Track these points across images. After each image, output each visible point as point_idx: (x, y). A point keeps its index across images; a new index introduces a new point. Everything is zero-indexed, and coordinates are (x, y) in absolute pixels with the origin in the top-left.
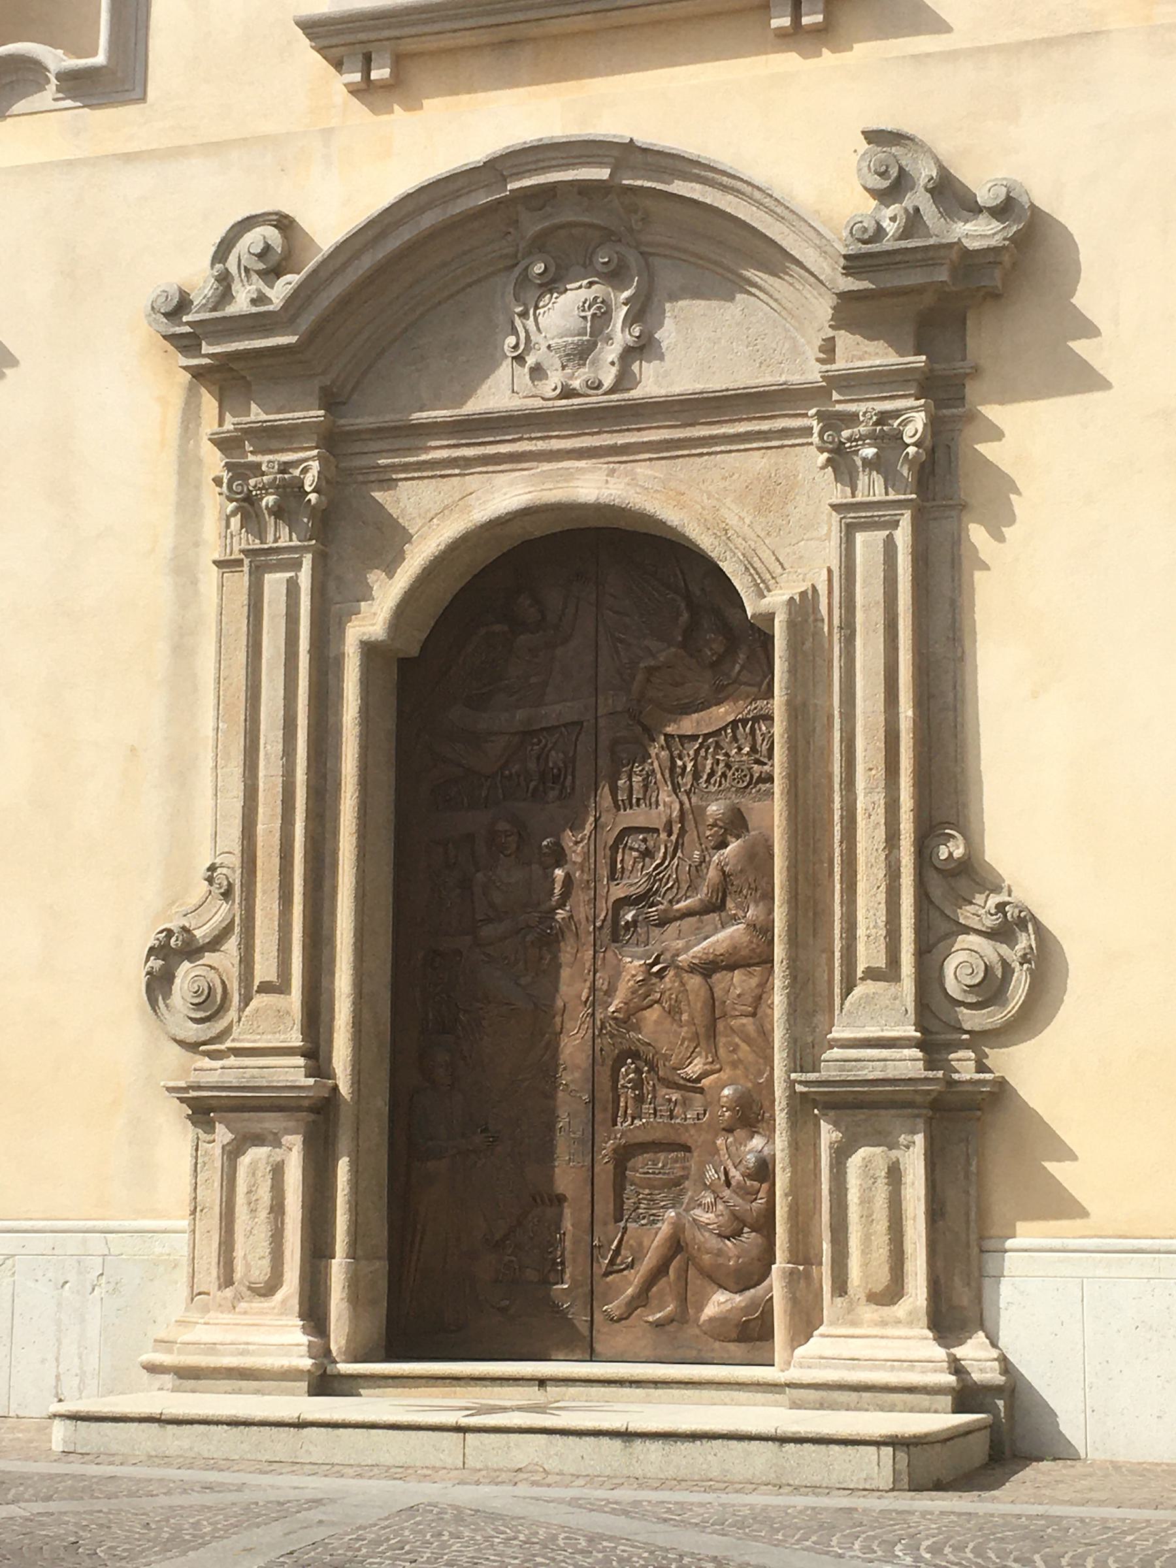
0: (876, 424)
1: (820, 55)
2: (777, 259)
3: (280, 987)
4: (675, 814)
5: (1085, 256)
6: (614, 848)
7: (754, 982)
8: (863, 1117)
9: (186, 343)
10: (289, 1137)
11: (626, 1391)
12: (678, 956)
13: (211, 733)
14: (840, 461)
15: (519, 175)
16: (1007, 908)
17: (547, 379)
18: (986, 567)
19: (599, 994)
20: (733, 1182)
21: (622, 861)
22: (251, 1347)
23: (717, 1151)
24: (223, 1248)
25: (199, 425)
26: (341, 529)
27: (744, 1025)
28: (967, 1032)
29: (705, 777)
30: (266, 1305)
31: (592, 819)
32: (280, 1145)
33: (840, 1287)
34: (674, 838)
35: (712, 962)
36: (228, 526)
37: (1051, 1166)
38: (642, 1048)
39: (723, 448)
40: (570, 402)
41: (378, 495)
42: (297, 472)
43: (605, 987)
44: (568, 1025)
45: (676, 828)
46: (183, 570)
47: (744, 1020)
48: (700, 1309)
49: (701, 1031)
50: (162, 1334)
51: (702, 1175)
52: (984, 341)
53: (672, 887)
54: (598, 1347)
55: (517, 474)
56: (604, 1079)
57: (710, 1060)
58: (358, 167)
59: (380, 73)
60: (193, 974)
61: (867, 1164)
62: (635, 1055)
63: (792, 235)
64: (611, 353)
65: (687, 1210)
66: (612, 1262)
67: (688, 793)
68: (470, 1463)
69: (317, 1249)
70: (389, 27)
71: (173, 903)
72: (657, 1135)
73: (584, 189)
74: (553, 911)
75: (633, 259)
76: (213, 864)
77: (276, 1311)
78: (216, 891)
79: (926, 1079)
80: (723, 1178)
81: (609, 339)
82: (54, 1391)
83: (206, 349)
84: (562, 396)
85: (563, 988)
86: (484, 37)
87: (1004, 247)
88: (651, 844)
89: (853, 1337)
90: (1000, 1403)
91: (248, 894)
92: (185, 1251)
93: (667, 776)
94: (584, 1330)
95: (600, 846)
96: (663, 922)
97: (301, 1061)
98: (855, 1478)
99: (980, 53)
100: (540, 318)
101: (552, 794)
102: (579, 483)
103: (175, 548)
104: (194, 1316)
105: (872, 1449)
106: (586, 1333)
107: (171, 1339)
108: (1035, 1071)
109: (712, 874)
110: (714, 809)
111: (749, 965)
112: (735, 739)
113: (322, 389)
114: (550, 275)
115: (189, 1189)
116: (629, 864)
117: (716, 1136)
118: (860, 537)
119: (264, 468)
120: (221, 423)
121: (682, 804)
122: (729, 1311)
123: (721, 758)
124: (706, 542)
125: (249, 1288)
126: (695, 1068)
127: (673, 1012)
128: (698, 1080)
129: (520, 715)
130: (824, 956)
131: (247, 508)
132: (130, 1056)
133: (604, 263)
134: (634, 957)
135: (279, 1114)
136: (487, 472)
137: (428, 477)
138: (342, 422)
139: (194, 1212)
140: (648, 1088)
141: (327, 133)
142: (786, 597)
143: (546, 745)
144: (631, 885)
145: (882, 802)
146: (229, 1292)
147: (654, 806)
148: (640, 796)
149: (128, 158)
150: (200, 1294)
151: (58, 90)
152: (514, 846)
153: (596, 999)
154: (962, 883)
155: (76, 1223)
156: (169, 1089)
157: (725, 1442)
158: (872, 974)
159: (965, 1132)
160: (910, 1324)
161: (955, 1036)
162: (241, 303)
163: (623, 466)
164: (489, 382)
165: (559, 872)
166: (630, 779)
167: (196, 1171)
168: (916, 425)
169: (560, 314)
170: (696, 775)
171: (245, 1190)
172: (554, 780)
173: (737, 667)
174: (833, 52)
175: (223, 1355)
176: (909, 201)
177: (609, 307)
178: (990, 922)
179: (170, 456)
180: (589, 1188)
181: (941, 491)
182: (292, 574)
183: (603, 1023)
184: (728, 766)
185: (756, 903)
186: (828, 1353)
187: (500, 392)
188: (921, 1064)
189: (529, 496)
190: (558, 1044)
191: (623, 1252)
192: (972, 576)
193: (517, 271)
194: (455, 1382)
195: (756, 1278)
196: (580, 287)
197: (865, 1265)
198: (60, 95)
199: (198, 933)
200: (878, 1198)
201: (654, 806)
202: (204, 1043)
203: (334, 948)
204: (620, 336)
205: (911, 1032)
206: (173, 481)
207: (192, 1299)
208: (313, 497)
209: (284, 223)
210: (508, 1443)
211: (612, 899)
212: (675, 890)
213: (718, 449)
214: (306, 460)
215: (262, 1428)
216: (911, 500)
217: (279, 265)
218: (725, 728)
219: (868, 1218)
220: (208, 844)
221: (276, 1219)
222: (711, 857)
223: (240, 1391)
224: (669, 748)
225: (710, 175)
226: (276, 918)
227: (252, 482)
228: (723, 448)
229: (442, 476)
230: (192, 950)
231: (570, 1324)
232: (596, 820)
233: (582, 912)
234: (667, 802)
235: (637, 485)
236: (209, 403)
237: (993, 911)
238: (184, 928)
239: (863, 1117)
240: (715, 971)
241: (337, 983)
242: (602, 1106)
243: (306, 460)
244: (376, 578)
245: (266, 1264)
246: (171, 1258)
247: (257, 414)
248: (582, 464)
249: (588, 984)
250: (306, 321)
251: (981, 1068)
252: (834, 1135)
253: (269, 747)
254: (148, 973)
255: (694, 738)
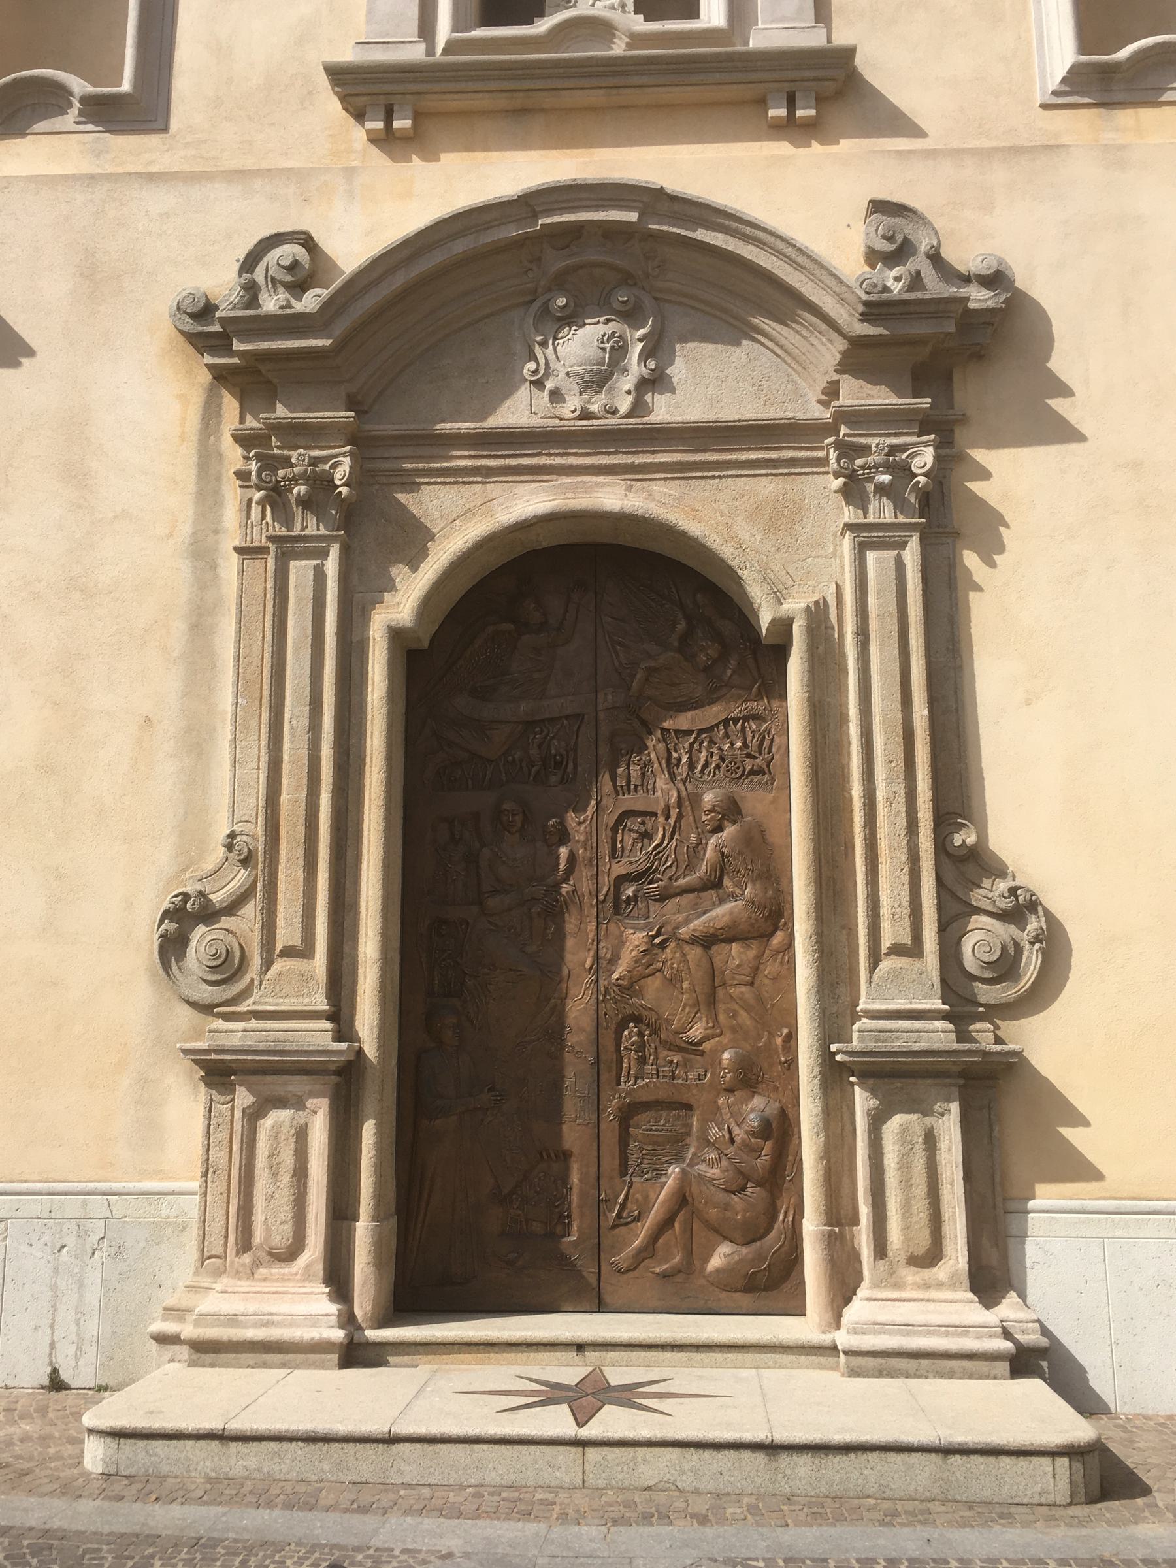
0: (888, 454)
1: (809, 146)
2: (786, 303)
3: (304, 951)
4: (673, 800)
5: (1059, 328)
6: (615, 830)
7: (752, 953)
8: (899, 1085)
9: (201, 342)
10: (315, 1101)
11: (668, 1355)
12: (678, 928)
13: (229, 708)
14: (853, 491)
15: (549, 212)
16: (1019, 892)
17: (564, 401)
18: (979, 589)
19: (604, 963)
20: (738, 1139)
21: (622, 841)
22: (275, 1318)
23: (719, 1109)
24: (241, 1213)
25: (219, 423)
26: (372, 531)
27: (742, 993)
28: (982, 1005)
29: (699, 768)
30: (286, 1271)
31: (593, 802)
32: (304, 1108)
33: (881, 1250)
34: (672, 821)
35: (712, 935)
36: (248, 516)
37: (1066, 1132)
38: (645, 1013)
39: (734, 472)
40: (591, 422)
41: (401, 497)
42: (327, 467)
43: (608, 956)
44: (571, 992)
45: (674, 813)
46: (202, 555)
47: (743, 989)
48: (706, 1259)
49: (702, 998)
50: (171, 1302)
51: (704, 1131)
52: (969, 392)
53: (671, 866)
54: (608, 1298)
55: (538, 484)
56: (608, 1041)
57: (710, 1025)
58: (377, 207)
59: (401, 124)
60: (210, 938)
61: (904, 1129)
62: (638, 1020)
63: (810, 283)
64: (627, 382)
65: (691, 1165)
66: (619, 1216)
67: (684, 781)
68: (591, 1480)
69: (341, 1212)
70: (415, 81)
71: (188, 868)
72: (661, 1095)
73: (611, 231)
74: (557, 886)
75: (647, 301)
76: (233, 831)
77: (298, 1277)
78: (234, 856)
79: (955, 1051)
80: (727, 1136)
81: (625, 370)
82: (47, 1360)
83: (237, 345)
84: (580, 418)
85: (569, 957)
86: (502, 102)
87: (1000, 309)
88: (649, 827)
89: (899, 1300)
90: (1044, 1364)
91: (271, 862)
92: (195, 1213)
93: (664, 765)
94: (593, 1280)
95: (602, 828)
96: (663, 898)
97: (328, 1025)
98: (1029, 1492)
99: (957, 154)
100: (559, 348)
101: (554, 779)
102: (596, 494)
103: (194, 534)
104: (205, 1281)
105: (1046, 1461)
106: (595, 1284)
107: (183, 1307)
108: (1049, 1043)
109: (710, 853)
110: (709, 798)
111: (747, 939)
112: (727, 735)
113: (348, 396)
114: (567, 312)
115: (200, 1150)
116: (629, 843)
117: (718, 1096)
118: (871, 556)
119: (293, 461)
120: (242, 420)
121: (679, 792)
122: (737, 1263)
123: (715, 751)
124: (726, 552)
125: (270, 1254)
126: (697, 1031)
127: (673, 981)
128: (700, 1043)
129: (523, 707)
130: (844, 932)
131: (276, 497)
132: (126, 1005)
133: (623, 302)
134: (636, 929)
135: (305, 1077)
136: (507, 482)
137: (450, 483)
138: (367, 427)
139: (205, 1174)
140: (650, 1049)
141: (350, 172)
142: (803, 605)
143: (548, 735)
144: (631, 863)
145: (903, 791)
146: (247, 1258)
147: (651, 792)
148: (638, 783)
149: (152, 178)
150: (210, 1258)
151: (81, 114)
152: (519, 825)
153: (601, 965)
154: (970, 869)
155: (76, 1184)
156: (186, 1052)
157: (883, 1455)
158: (897, 950)
159: (999, 1114)
160: (953, 1285)
161: (973, 1009)
162: (271, 304)
163: (639, 484)
164: (508, 403)
165: (563, 851)
166: (628, 768)
167: (208, 1132)
168: (924, 458)
169: (580, 345)
170: (691, 766)
171: (267, 1153)
172: (556, 768)
173: (729, 672)
174: (822, 144)
175: (245, 1327)
176: (911, 265)
177: (625, 341)
178: (1005, 904)
179: (189, 452)
180: (595, 1144)
181: (943, 525)
182: (318, 562)
183: (607, 989)
184: (722, 759)
185: (753, 881)
186: (881, 1318)
187: (518, 411)
188: (953, 1036)
189: (555, 503)
190: (564, 1006)
191: (629, 1205)
192: (967, 596)
193: (537, 305)
194: (489, 1348)
195: (762, 1231)
196: (598, 322)
197: (906, 1228)
198: (82, 119)
199: (215, 898)
200: (915, 1163)
201: (651, 792)
202: (219, 1005)
203: (357, 914)
204: (635, 367)
205: (937, 1004)
206: (192, 473)
207: (203, 1263)
208: (344, 490)
209: (307, 241)
210: (634, 1459)
211: (613, 876)
212: (674, 869)
213: (730, 473)
214: (337, 456)
215: (345, 1445)
216: (921, 524)
217: (305, 282)
218: (717, 725)
219: (906, 1183)
220: (225, 813)
221: (299, 1182)
222: (708, 840)
223: (265, 1365)
224: (665, 741)
225: (735, 225)
226: (301, 885)
227: (281, 473)
228: (734, 472)
229: (464, 483)
230: (208, 914)
231: (580, 1276)
232: (598, 803)
233: (585, 886)
234: (664, 790)
235: (654, 500)
236: (230, 405)
237: (1006, 895)
238: (200, 892)
239: (899, 1085)
240: (713, 944)
241: (361, 948)
242: (606, 1067)
243: (337, 456)
244: (399, 572)
245: (288, 1229)
246: (180, 1220)
247: (281, 411)
248: (600, 479)
249: (592, 953)
250: (341, 327)
251: (998, 1040)
252: (871, 1102)
253: (294, 722)
254: (161, 936)
255: (689, 733)
